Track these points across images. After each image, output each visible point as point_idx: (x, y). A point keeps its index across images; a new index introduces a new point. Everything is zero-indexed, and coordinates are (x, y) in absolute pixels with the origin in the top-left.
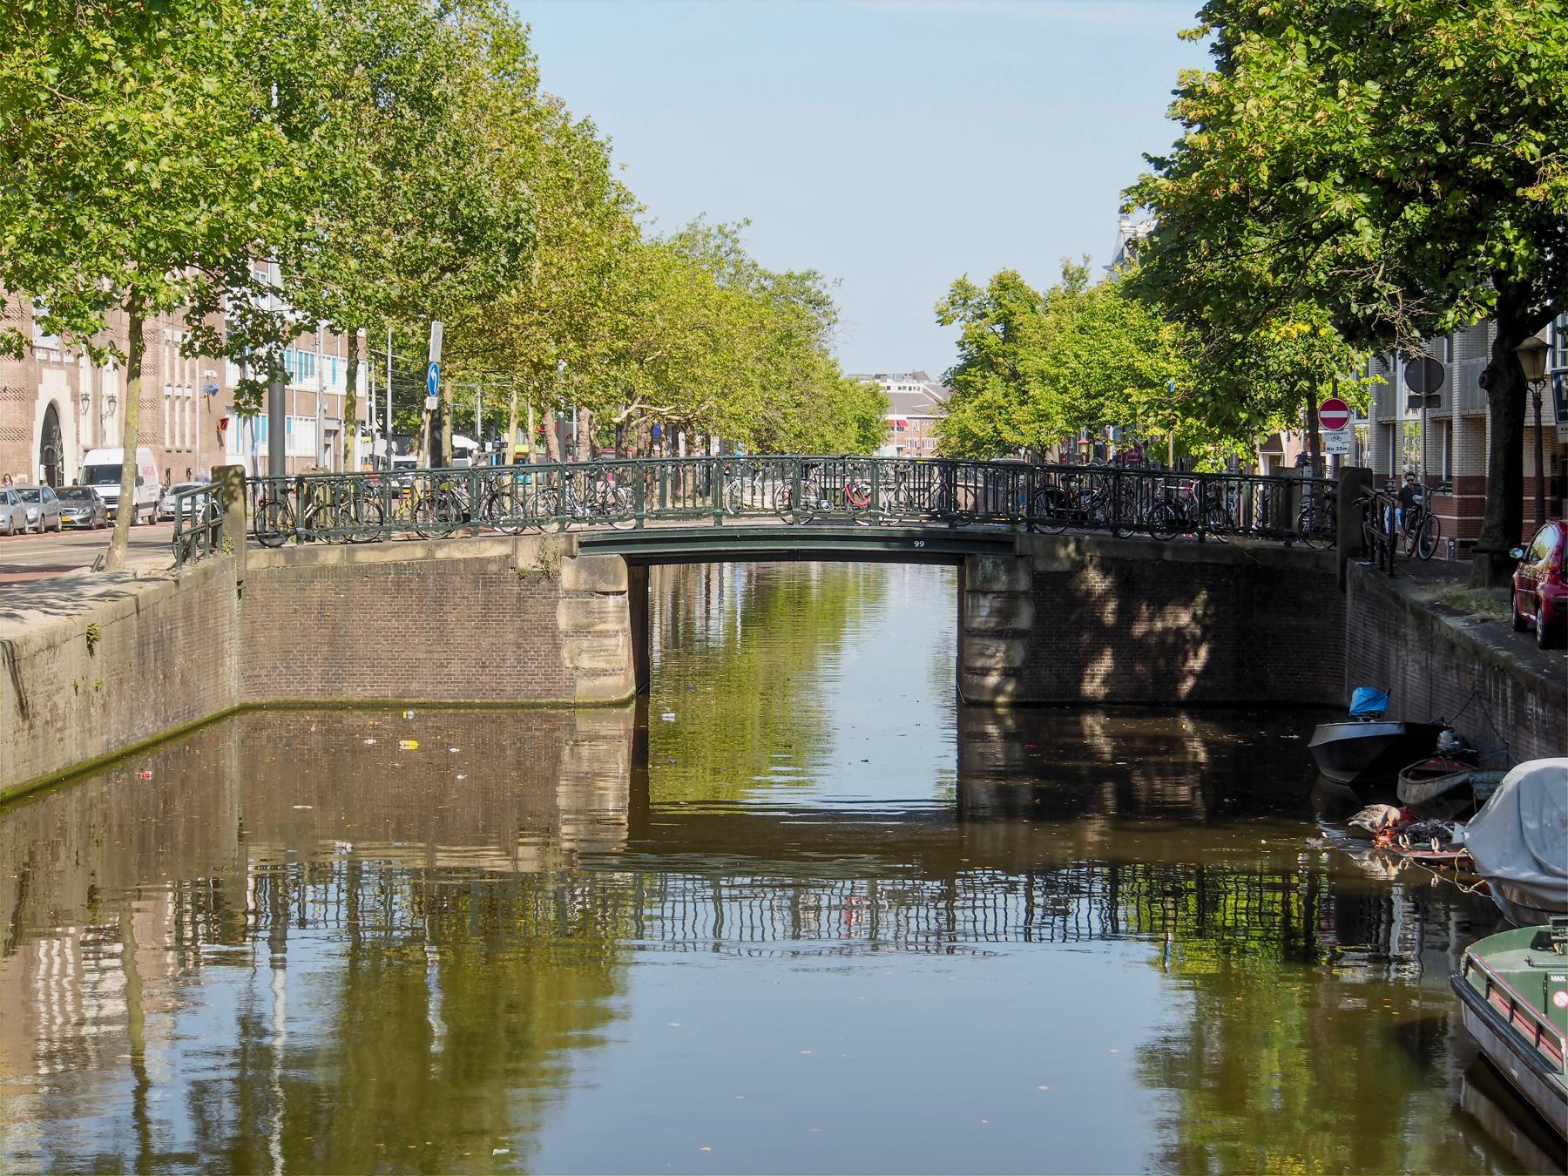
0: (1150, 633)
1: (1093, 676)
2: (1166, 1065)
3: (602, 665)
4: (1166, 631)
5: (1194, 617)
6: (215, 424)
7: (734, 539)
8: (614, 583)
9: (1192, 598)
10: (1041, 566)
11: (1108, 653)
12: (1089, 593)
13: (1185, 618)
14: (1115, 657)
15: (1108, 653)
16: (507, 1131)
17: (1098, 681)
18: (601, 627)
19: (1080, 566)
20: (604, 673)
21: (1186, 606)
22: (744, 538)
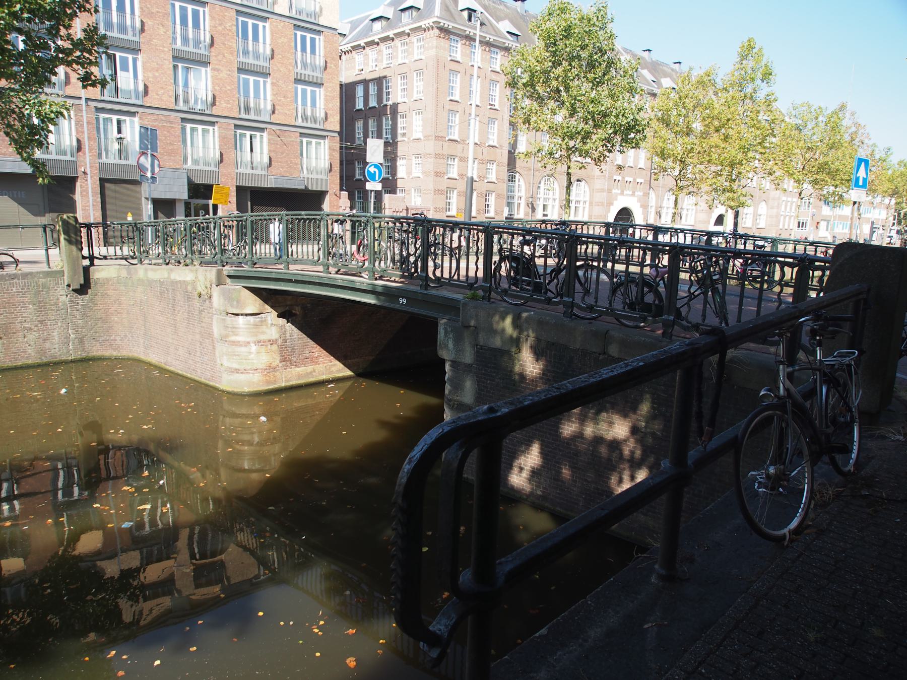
0: (579, 436)
1: (521, 469)
2: (81, 285)
3: (235, 366)
4: (598, 440)
5: (634, 430)
6: (815, 224)
7: (290, 281)
8: (237, 307)
9: (634, 409)
10: (481, 341)
11: (535, 449)
12: (522, 376)
13: (619, 429)
14: (543, 453)
15: (535, 449)
16: (175, 553)
17: (525, 474)
18: (233, 338)
19: (517, 343)
20: (237, 371)
21: (625, 416)
22: (297, 282)
